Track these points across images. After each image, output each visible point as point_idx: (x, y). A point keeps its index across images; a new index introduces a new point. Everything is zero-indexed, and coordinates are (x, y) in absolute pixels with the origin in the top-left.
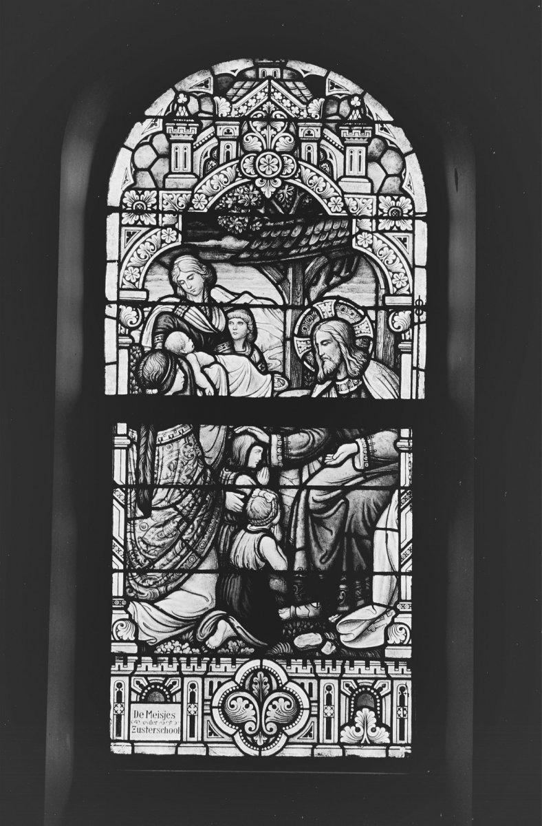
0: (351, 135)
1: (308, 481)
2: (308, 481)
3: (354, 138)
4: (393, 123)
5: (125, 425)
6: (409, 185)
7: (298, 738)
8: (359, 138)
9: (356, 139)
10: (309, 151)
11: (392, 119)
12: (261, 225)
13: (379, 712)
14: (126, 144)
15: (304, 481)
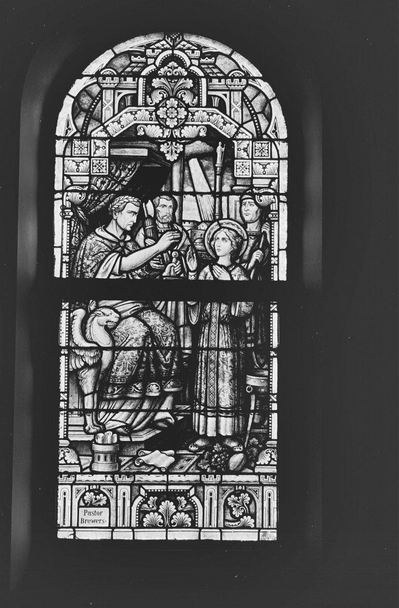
0: (104, 81)
1: (191, 489)
2: (191, 489)
3: (107, 84)
4: (263, 79)
5: (190, 278)
6: (273, 132)
7: (258, 498)
8: (110, 84)
9: (108, 85)
10: (118, 367)
11: (261, 75)
12: (215, 447)
13: (256, 121)
14: (70, 93)
15: (193, 489)
